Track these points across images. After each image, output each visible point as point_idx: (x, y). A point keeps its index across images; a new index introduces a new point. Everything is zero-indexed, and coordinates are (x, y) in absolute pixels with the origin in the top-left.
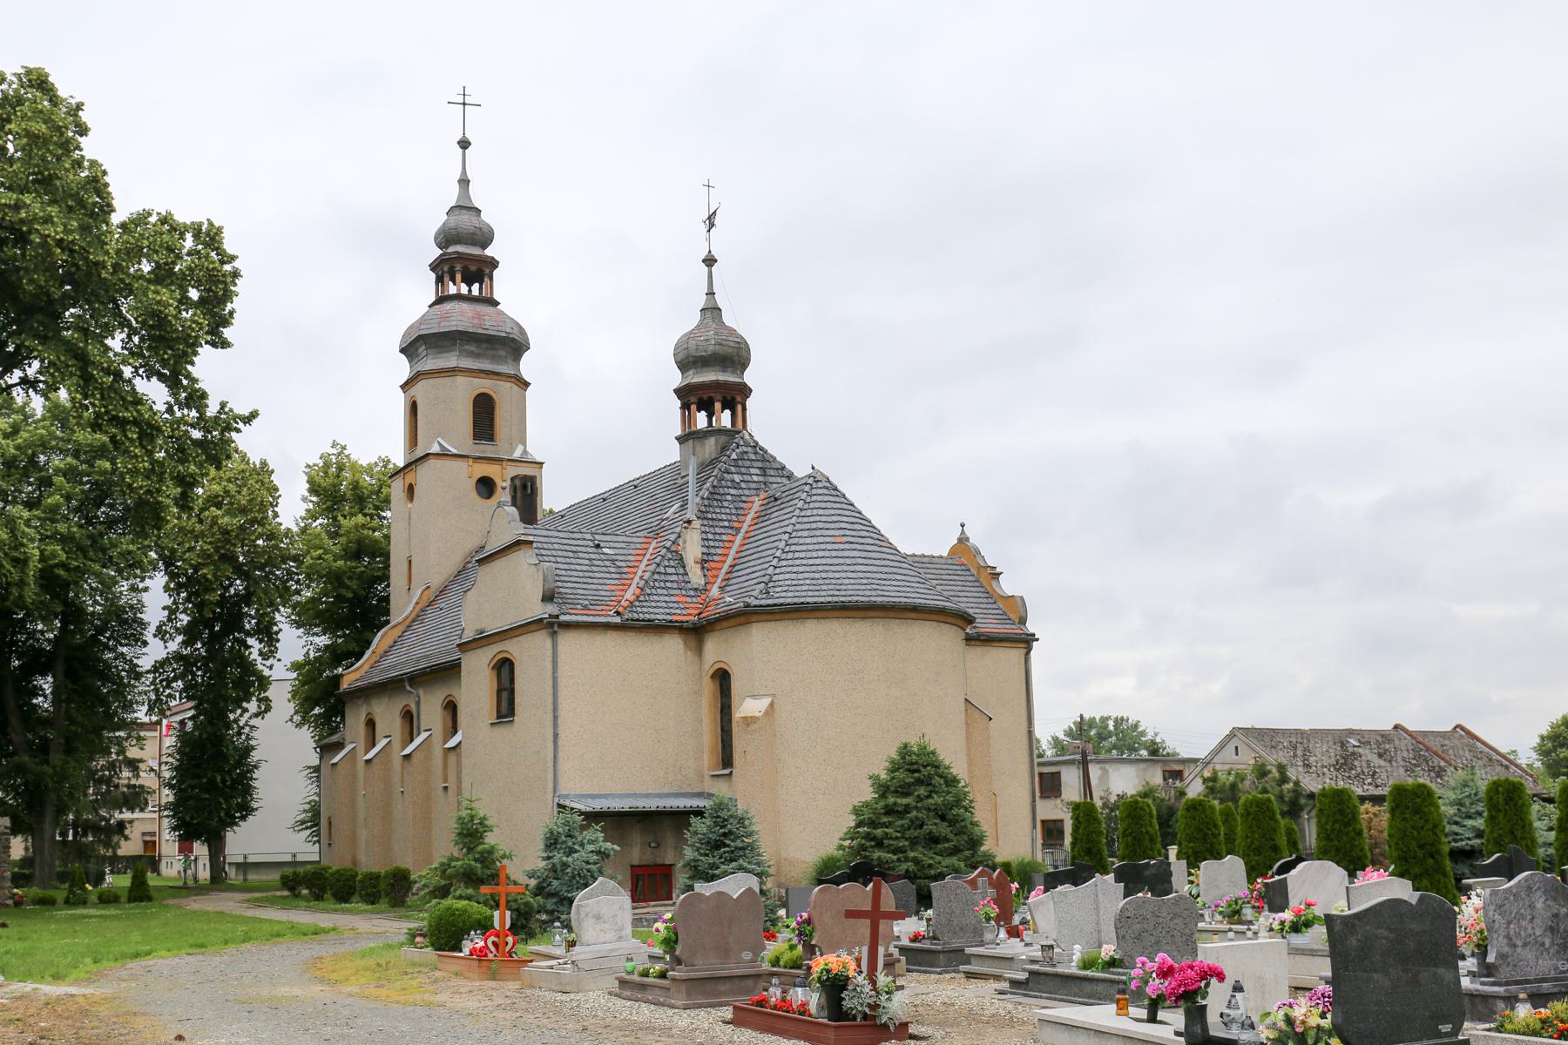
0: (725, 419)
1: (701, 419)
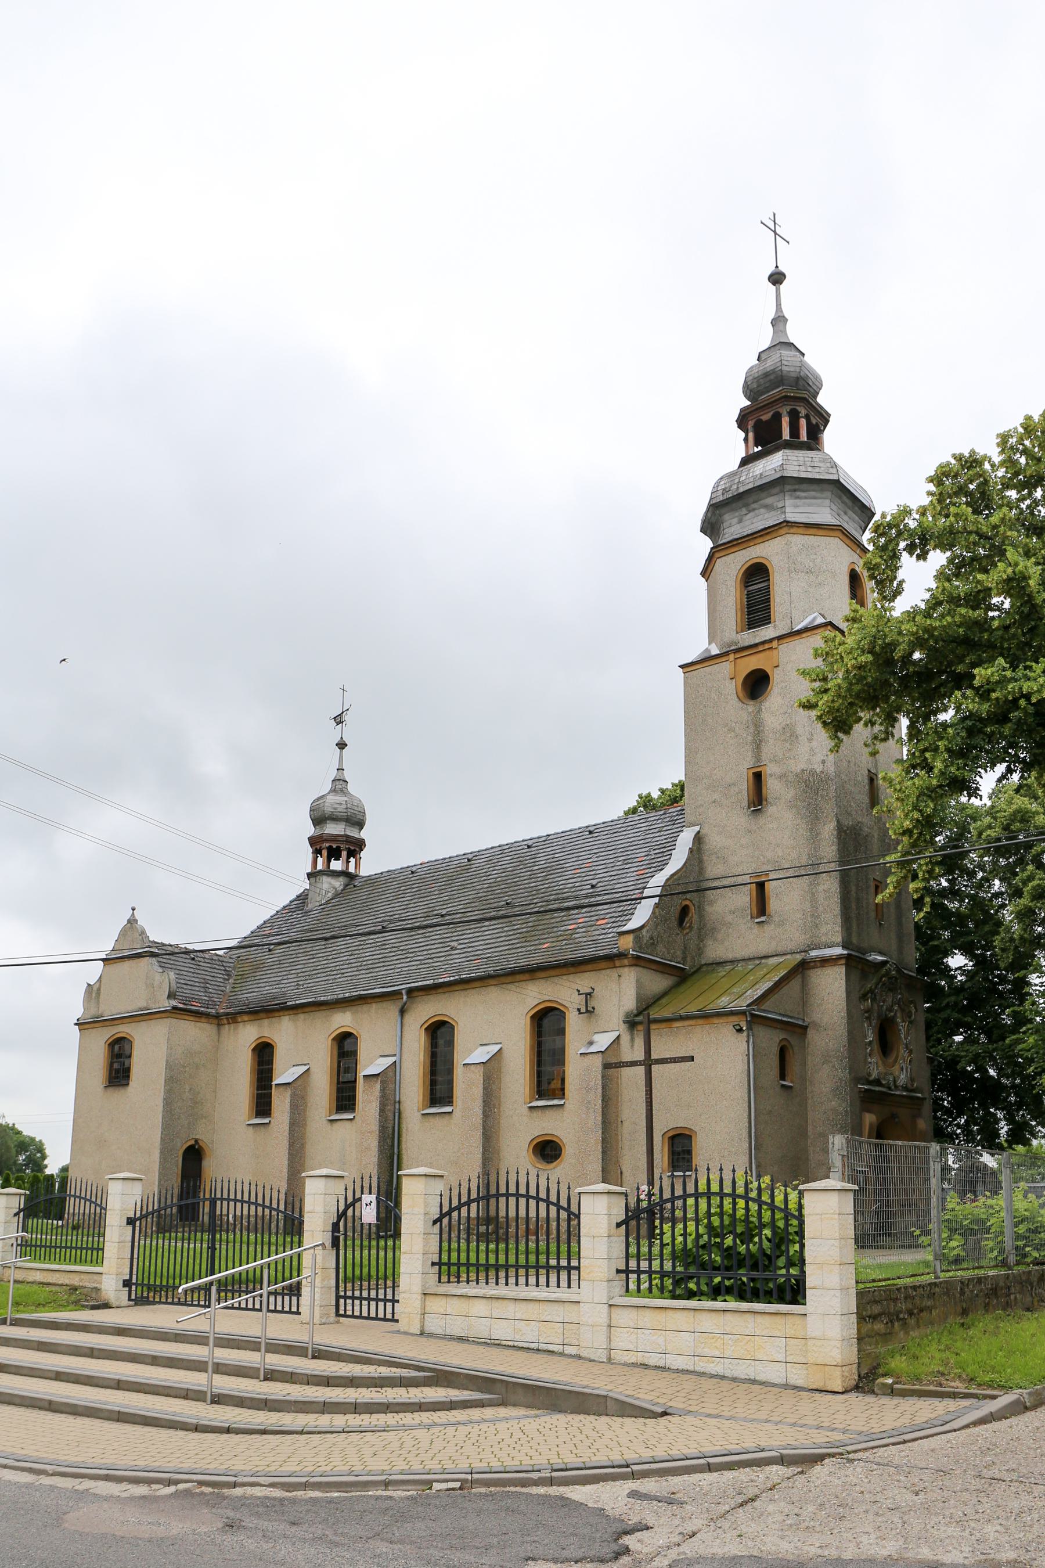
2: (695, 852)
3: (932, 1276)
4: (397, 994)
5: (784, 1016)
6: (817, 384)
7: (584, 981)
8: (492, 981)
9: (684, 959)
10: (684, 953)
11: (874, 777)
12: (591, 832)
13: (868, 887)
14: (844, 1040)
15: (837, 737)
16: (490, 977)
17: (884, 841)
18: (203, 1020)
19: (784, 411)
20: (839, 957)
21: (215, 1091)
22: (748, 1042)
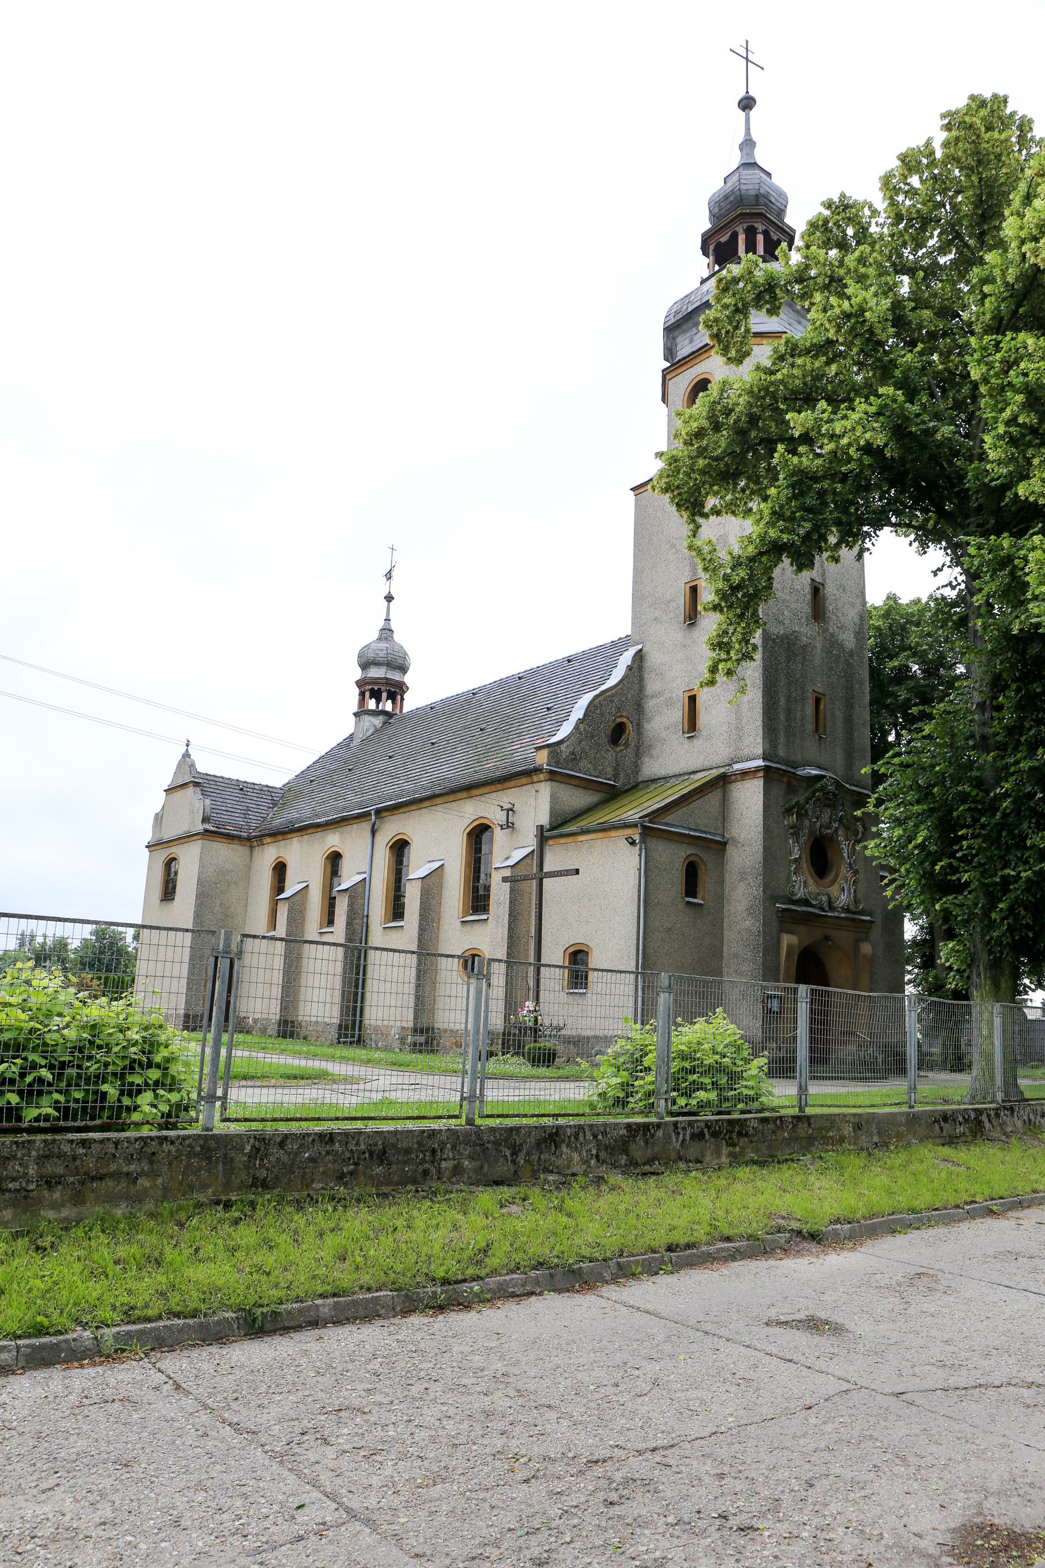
0: (388, 706)
1: (372, 704)
2: (635, 670)
3: (797, 1109)
4: (367, 815)
5: (695, 830)
6: (781, 200)
7: (506, 797)
8: (439, 801)
9: (616, 777)
10: (615, 769)
11: (821, 587)
12: (569, 661)
13: (804, 699)
14: (760, 857)
15: (694, 521)
16: (434, 796)
17: (831, 652)
18: (235, 842)
19: (740, 230)
20: (757, 770)
21: (246, 906)
22: (640, 855)
